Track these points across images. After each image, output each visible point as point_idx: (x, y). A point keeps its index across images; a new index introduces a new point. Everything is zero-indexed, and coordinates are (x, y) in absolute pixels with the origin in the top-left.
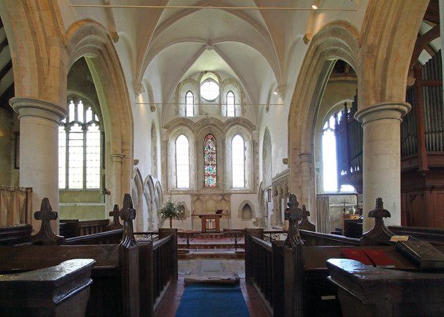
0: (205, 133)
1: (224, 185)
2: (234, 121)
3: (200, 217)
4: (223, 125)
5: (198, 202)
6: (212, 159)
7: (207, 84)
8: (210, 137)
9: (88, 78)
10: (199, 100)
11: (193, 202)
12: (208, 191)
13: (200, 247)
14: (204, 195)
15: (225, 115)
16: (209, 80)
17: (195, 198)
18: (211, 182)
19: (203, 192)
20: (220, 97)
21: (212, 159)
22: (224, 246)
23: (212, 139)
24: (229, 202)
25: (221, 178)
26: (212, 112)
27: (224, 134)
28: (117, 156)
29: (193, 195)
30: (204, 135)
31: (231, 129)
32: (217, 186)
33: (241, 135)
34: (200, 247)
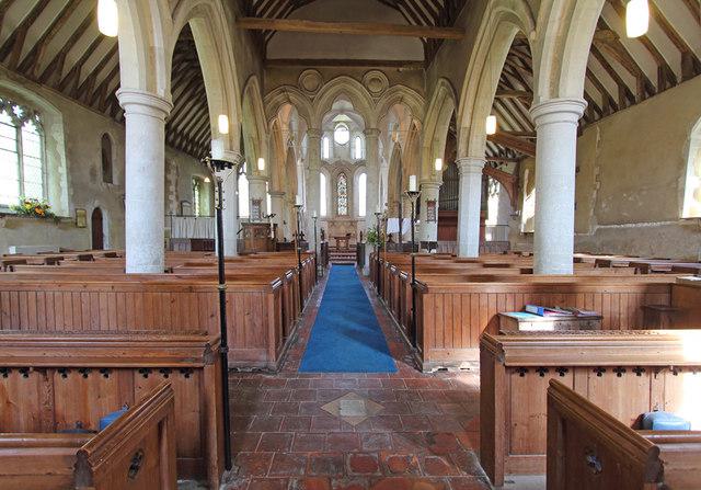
2: (361, 163)
20: (350, 142)
29: (329, 222)
32: (348, 215)
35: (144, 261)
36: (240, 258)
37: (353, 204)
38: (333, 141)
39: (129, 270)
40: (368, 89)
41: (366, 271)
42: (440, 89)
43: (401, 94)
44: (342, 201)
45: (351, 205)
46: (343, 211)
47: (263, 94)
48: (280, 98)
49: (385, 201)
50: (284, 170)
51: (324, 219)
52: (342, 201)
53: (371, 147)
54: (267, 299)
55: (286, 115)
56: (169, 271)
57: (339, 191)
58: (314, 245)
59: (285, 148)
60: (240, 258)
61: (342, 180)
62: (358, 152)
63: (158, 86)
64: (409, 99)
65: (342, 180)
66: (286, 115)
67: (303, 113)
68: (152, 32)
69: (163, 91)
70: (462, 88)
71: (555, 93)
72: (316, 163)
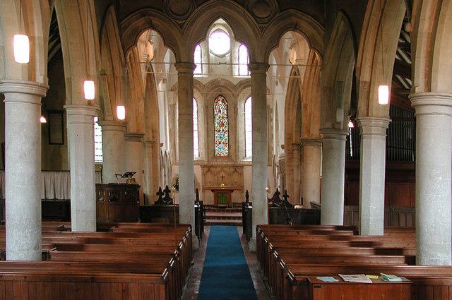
0: (215, 93)
1: (236, 156)
2: (243, 84)
3: (212, 191)
4: (235, 87)
5: (209, 174)
6: (222, 125)
7: (217, 34)
8: (221, 98)
9: (347, 177)
10: (208, 56)
11: (204, 174)
12: (219, 162)
13: (214, 218)
14: (216, 167)
15: (237, 73)
16: (218, 30)
17: (206, 169)
18: (222, 150)
19: (215, 163)
20: (231, 52)
21: (222, 125)
22: (234, 218)
23: (223, 101)
24: (241, 174)
25: (233, 147)
26: (220, 71)
27: (236, 97)
28: (150, 142)
29: (203, 167)
30: (215, 96)
31: (243, 92)
32: (229, 156)
33: (295, 27)
34: (214, 218)
35: (25, 247)
36: (100, 235)
37: (236, 141)
38: (208, 51)
39: (11, 257)
40: (253, 14)
41: (253, 246)
42: (340, 25)
43: (294, 19)
44: (221, 137)
45: (234, 143)
46: (222, 150)
47: (119, 20)
48: (141, 21)
49: (282, 142)
50: (142, 103)
51: (198, 163)
52: (221, 137)
53: (259, 66)
54: (159, 289)
55: (148, 46)
56: (45, 256)
57: (217, 121)
58: (187, 215)
59: (144, 73)
60: (100, 235)
61: (221, 106)
62: (242, 70)
63: (38, 73)
64: (304, 25)
65: (221, 106)
66: (148, 46)
67: (168, 41)
68: (32, 23)
69: (42, 77)
70: (360, 32)
71: (428, 87)
72: (186, 86)
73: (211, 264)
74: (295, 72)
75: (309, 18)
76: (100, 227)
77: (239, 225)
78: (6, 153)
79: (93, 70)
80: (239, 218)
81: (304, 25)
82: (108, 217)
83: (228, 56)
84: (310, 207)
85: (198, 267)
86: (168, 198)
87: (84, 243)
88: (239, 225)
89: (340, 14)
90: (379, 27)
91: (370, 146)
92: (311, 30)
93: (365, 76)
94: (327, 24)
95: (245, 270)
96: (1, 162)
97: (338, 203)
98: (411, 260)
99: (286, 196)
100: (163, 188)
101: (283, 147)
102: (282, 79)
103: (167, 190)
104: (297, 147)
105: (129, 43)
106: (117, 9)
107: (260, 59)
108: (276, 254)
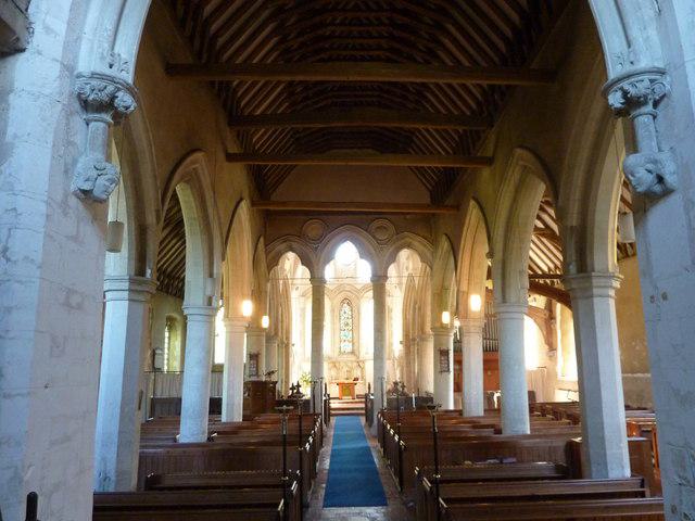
2: (365, 288)
4: (358, 291)
25: (356, 344)
32: (353, 353)
33: (409, 246)
36: (246, 424)
40: (374, 237)
41: (374, 430)
42: (445, 245)
48: (283, 246)
55: (290, 263)
60: (246, 424)
65: (346, 308)
66: (290, 263)
73: (336, 447)
74: (411, 277)
75: (419, 238)
76: (245, 418)
77: (362, 414)
78: (291, 359)
79: (247, 289)
80: (362, 409)
81: (416, 244)
82: (248, 413)
83: (352, 266)
84: (425, 396)
85: (327, 450)
86: (298, 392)
87: (234, 430)
88: (362, 414)
89: (444, 237)
90: (515, 200)
91: (469, 343)
92: (421, 247)
93: (464, 287)
94: (434, 243)
95: (367, 452)
96: (98, 362)
97: (448, 391)
98: (461, 414)
99: (403, 387)
100: (295, 384)
101: (401, 343)
102: (400, 284)
103: (299, 386)
104: (412, 341)
105: (274, 261)
106: (265, 238)
107: (381, 273)
108: (396, 438)
